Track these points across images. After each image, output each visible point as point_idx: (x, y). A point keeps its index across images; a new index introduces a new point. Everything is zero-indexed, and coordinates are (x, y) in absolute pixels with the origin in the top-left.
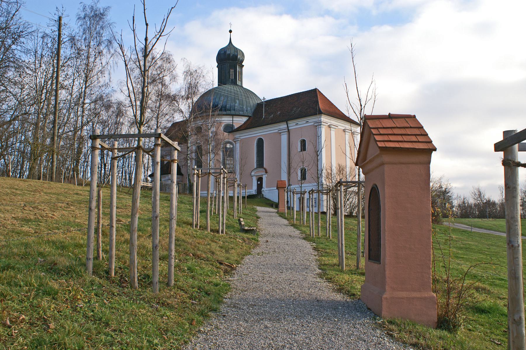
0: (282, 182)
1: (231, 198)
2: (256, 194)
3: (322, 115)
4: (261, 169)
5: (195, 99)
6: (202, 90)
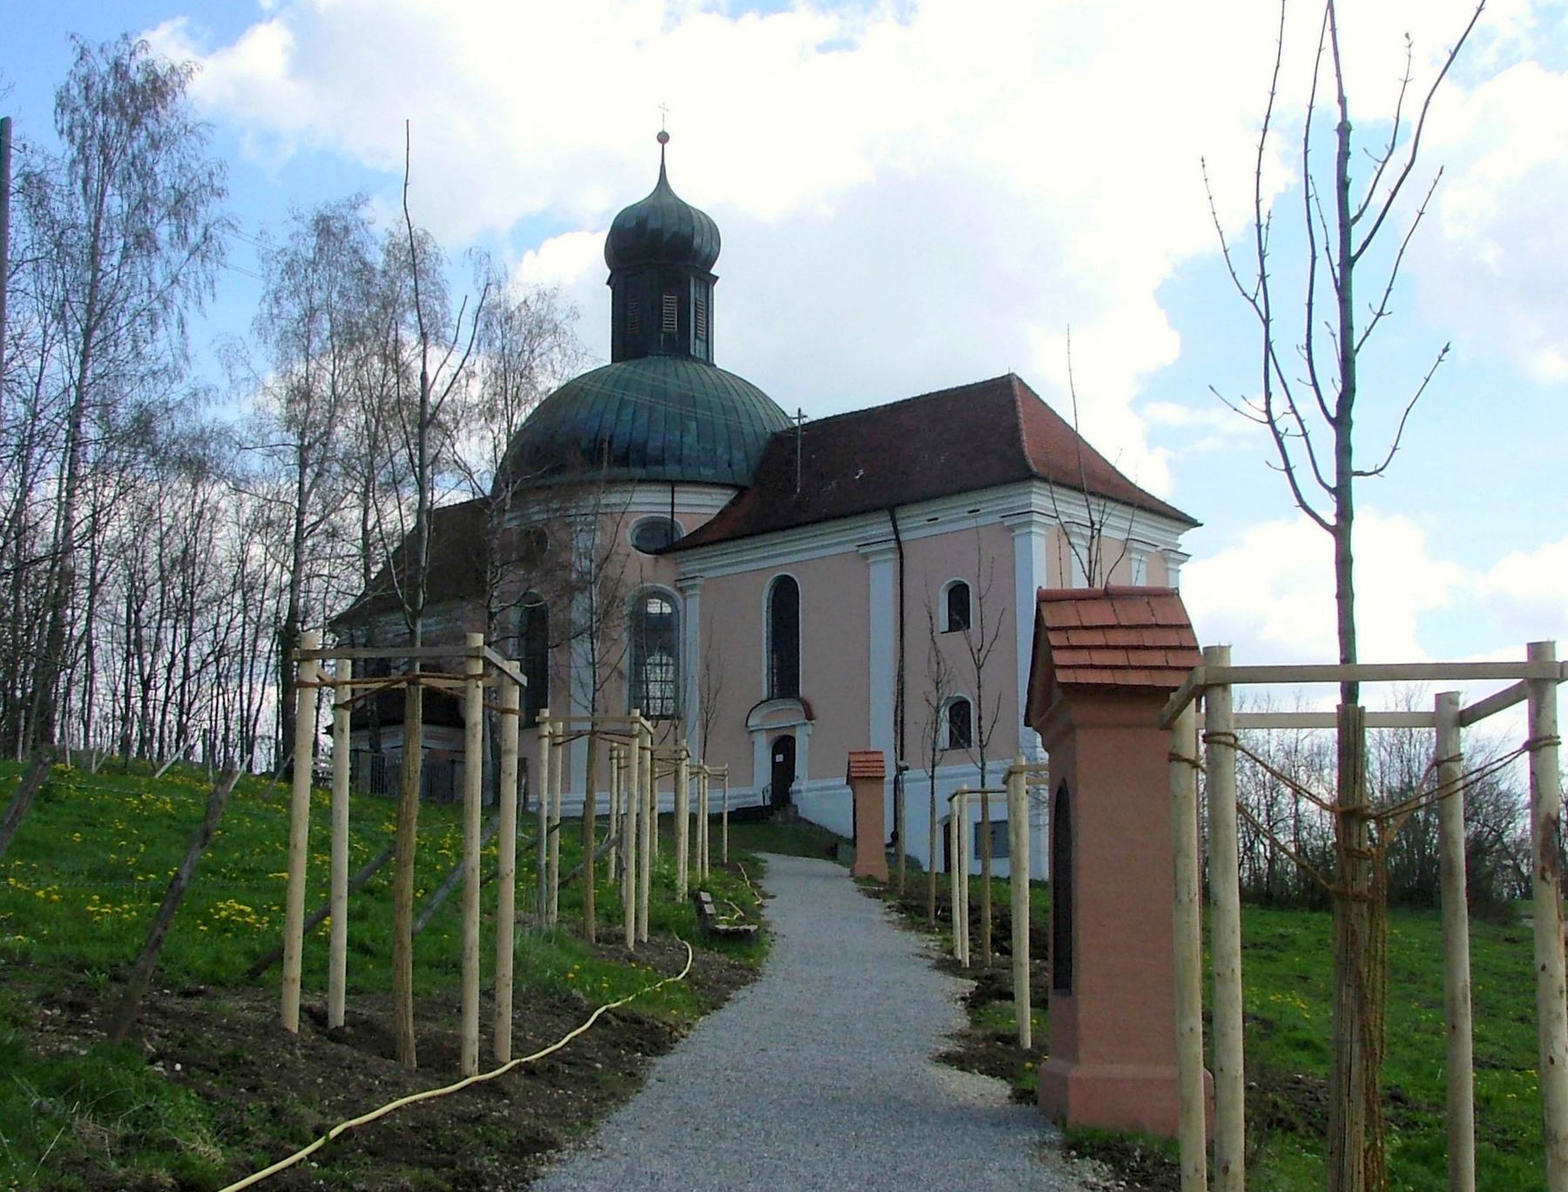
0: (870, 757)
1: (667, 821)
2: (768, 803)
3: (1036, 483)
4: (789, 704)
5: (520, 419)
6: (548, 382)
